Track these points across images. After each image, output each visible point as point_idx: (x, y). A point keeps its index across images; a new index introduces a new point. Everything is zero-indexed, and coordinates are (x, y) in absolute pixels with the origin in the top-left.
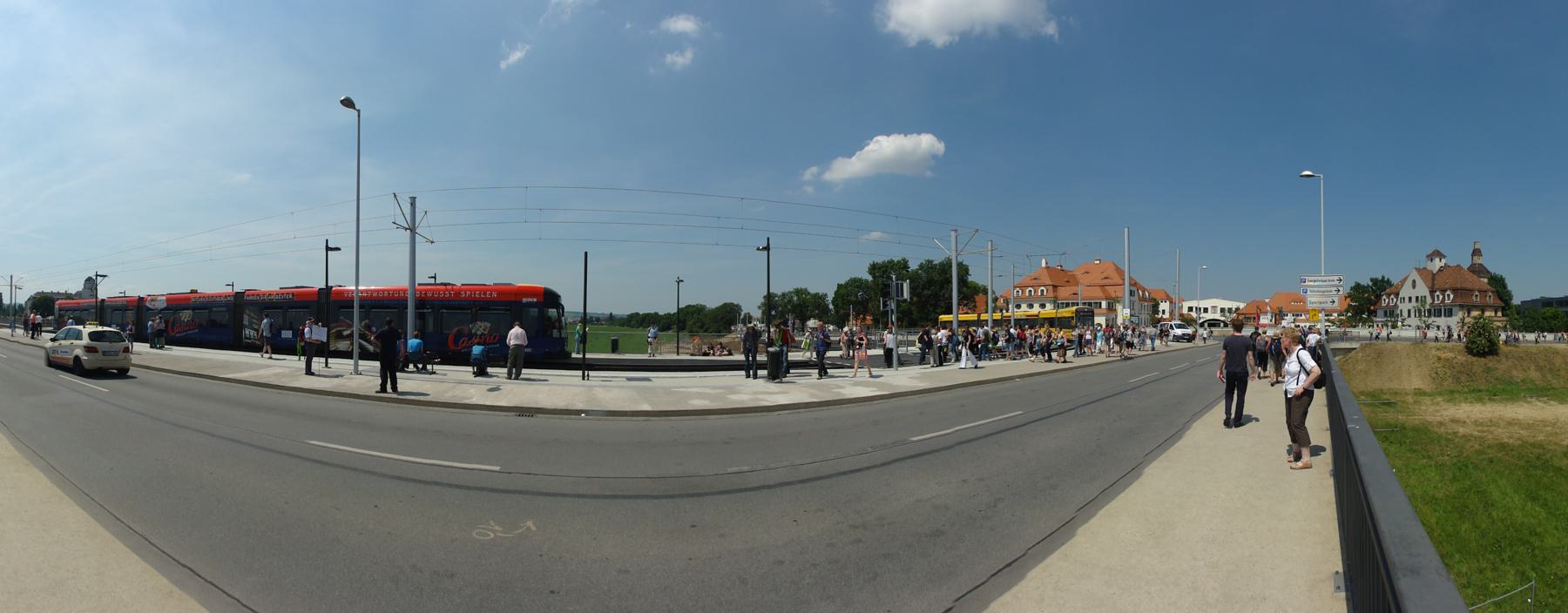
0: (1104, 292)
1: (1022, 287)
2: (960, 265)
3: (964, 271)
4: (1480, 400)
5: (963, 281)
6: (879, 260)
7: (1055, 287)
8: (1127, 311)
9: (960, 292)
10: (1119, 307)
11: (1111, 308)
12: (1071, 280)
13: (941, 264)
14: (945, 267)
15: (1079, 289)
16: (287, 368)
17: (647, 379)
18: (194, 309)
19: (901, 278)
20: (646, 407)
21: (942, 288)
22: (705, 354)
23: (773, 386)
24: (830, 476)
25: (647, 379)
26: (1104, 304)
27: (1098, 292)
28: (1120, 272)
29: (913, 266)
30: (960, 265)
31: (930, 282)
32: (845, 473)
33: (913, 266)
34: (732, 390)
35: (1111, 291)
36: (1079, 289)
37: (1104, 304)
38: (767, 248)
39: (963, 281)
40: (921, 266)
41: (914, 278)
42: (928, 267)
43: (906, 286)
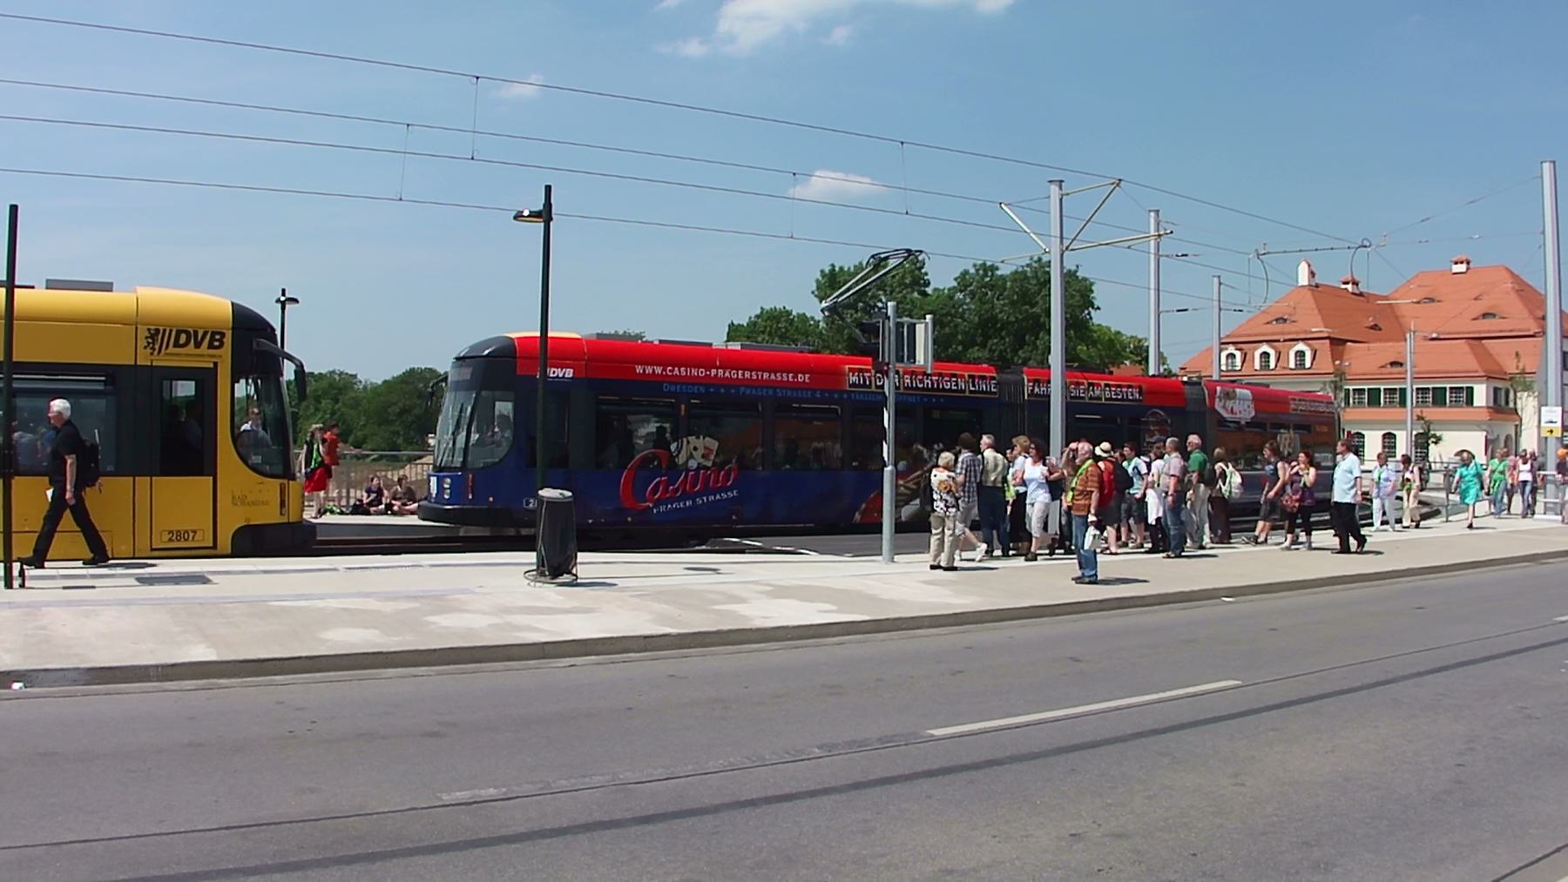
0: (1484, 357)
1: (1244, 344)
2: (1070, 278)
3: (1080, 295)
4: (828, 589)
5: (1077, 326)
6: (850, 257)
7: (1337, 343)
8: (1553, 414)
9: (1070, 357)
10: (1526, 404)
11: (1502, 407)
12: (1380, 319)
13: (1019, 276)
14: (1033, 282)
15: (1408, 349)
16: (492, 595)
17: (201, 579)
18: (1298, 427)
19: (908, 310)
20: (202, 653)
21: (1020, 343)
22: (359, 509)
23: (550, 593)
24: (715, 810)
25: (201, 579)
26: (1481, 395)
27: (1461, 357)
28: (1531, 298)
29: (941, 277)
30: (1070, 278)
31: (988, 326)
32: (752, 803)
33: (941, 277)
34: (441, 602)
35: (1505, 355)
36: (1408, 349)
37: (1481, 395)
38: (545, 215)
39: (1077, 326)
40: (964, 280)
41: (945, 313)
42: (982, 282)
43: (923, 333)
